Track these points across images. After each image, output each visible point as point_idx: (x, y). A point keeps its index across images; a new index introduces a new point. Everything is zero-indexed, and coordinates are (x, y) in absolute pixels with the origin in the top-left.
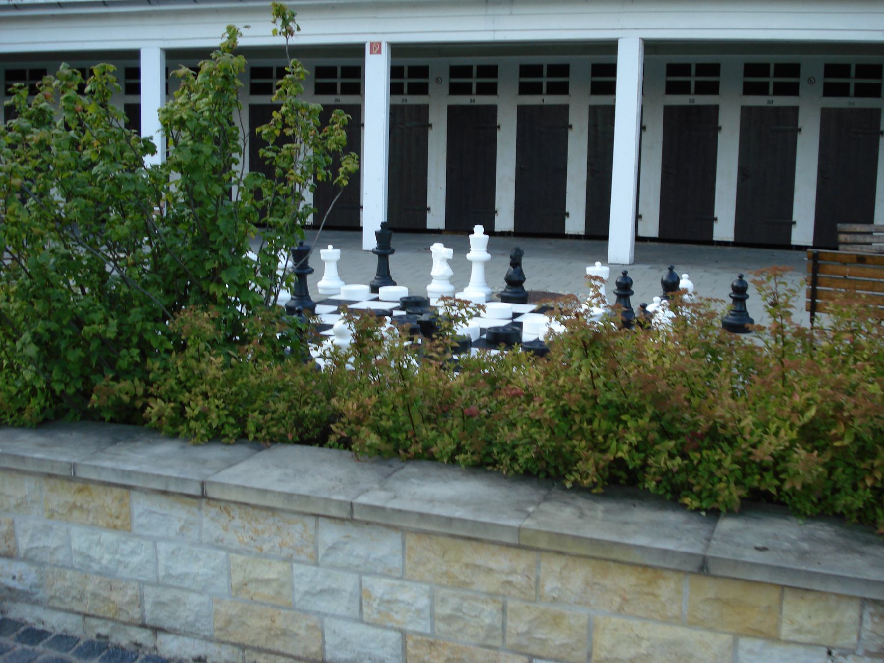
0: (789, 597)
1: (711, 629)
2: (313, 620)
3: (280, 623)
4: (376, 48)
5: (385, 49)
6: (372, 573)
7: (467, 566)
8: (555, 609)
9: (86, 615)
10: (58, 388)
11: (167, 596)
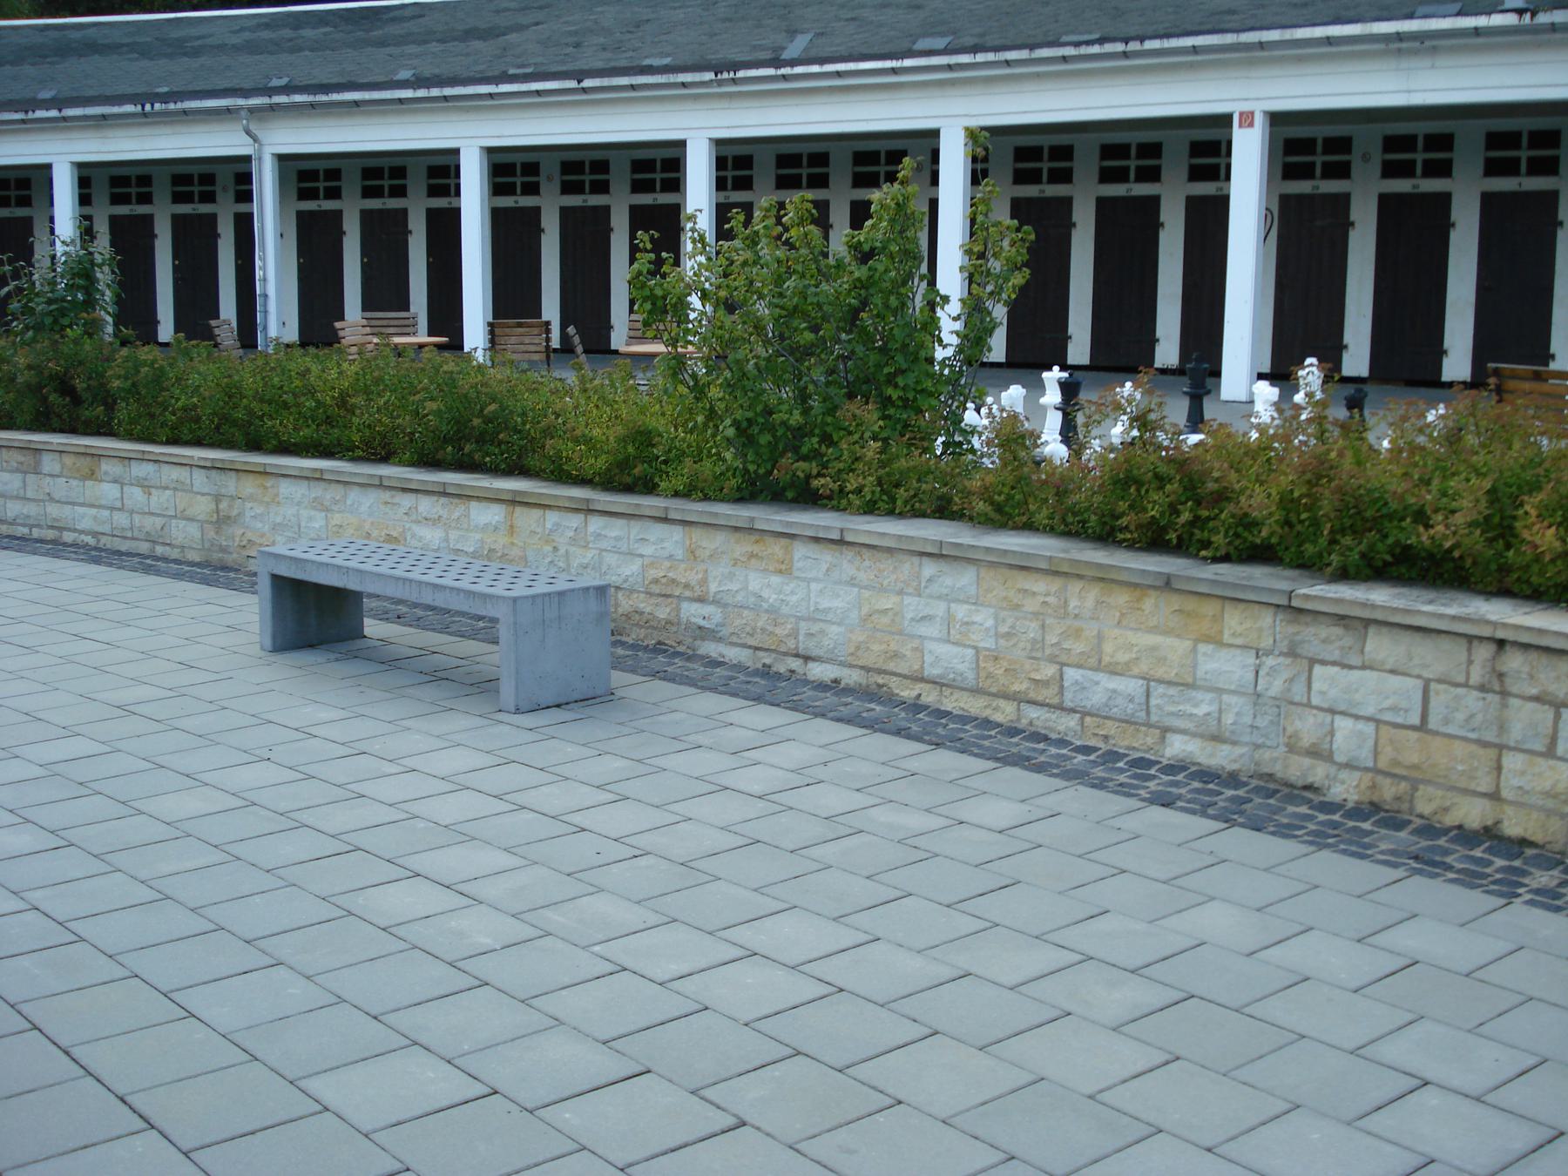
0: (1228, 606)
1: (1178, 636)
2: (916, 643)
3: (893, 646)
4: (1247, 119)
5: (1259, 119)
6: (957, 601)
7: (1019, 590)
8: (1077, 624)
9: (757, 649)
10: (752, 468)
11: (815, 628)
